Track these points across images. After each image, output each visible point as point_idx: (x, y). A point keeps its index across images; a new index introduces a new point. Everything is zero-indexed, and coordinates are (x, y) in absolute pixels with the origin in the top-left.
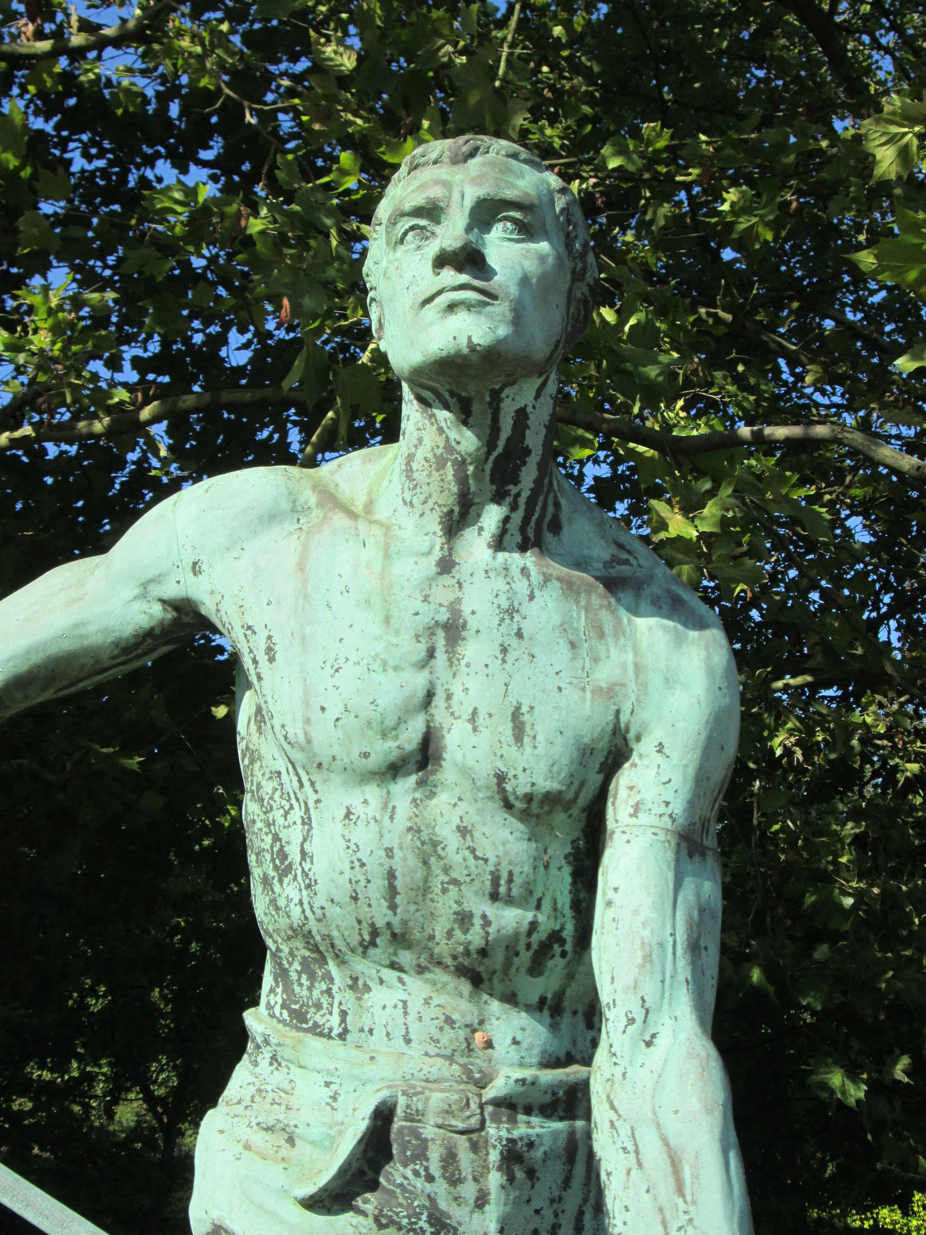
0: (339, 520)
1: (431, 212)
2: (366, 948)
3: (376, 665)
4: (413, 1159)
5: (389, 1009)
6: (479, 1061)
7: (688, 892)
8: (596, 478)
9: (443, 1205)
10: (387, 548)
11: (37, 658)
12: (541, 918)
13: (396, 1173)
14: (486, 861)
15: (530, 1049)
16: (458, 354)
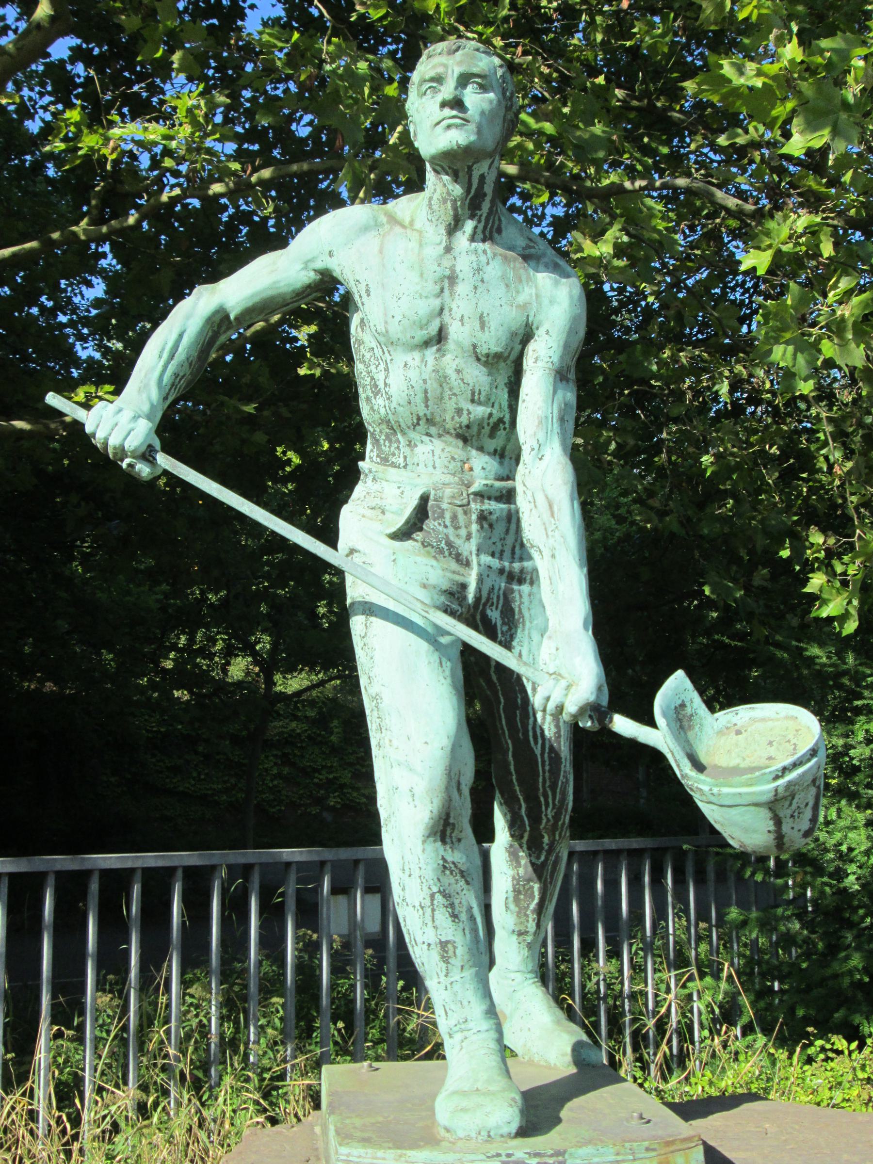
0: (398, 229)
1: (438, 80)
3: (417, 296)
4: (438, 518)
6: (467, 477)
7: (560, 394)
8: (552, 216)
9: (452, 538)
10: (421, 241)
11: (257, 299)
12: (494, 411)
13: (430, 524)
15: (490, 471)
16: (452, 149)
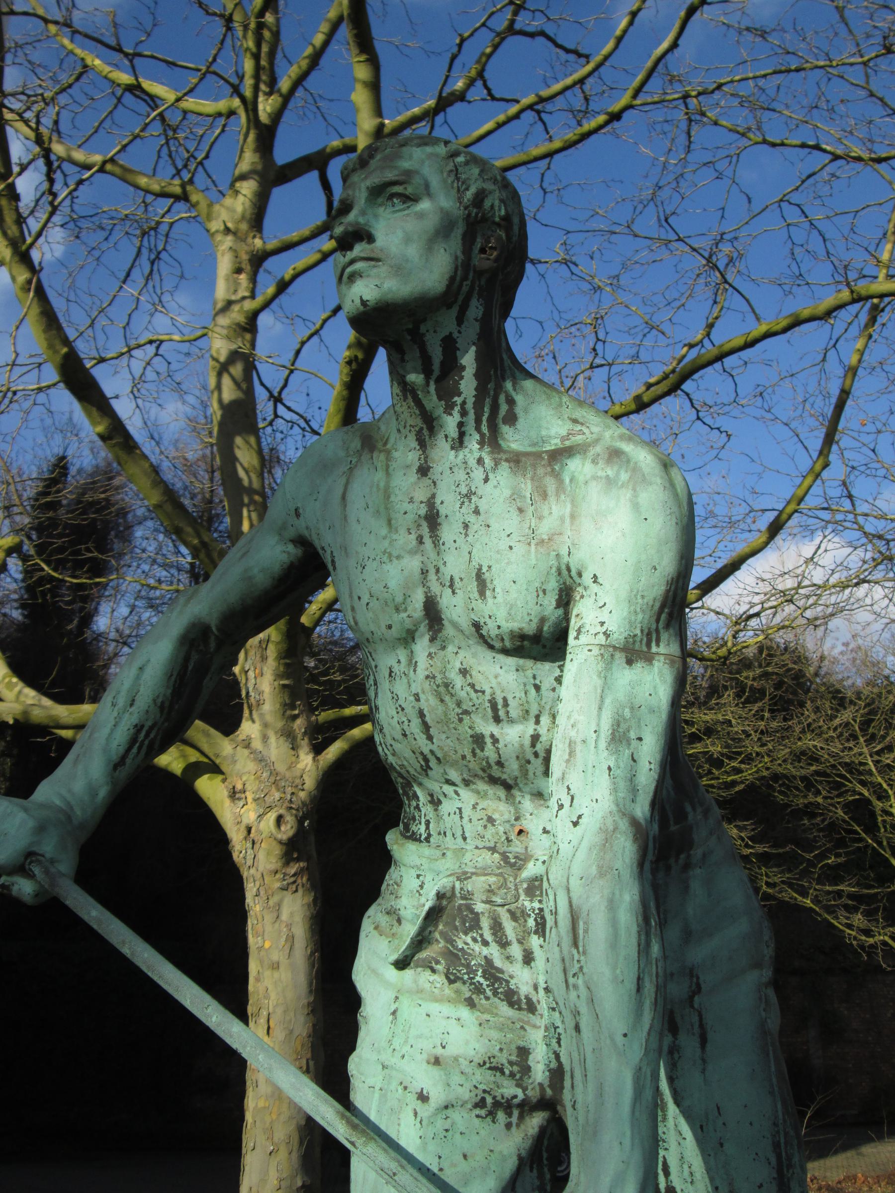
2: (426, 771)
3: (385, 559)
4: (471, 929)
5: (452, 815)
9: (498, 962)
14: (483, 692)
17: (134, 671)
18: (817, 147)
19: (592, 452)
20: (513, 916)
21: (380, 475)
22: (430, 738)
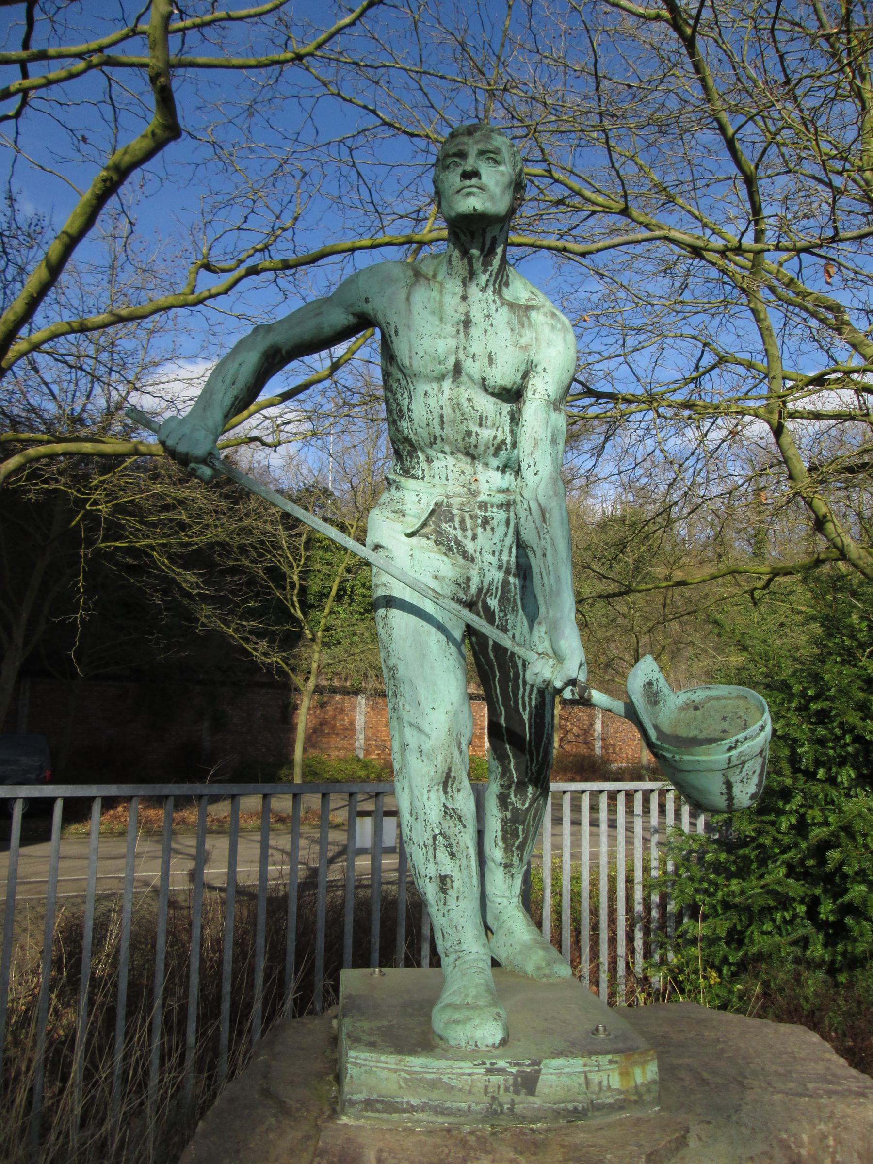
9: (460, 538)
17: (236, 365)
18: (374, 112)
19: (542, 310)
20: (471, 517)
21: (435, 294)
22: (442, 429)
